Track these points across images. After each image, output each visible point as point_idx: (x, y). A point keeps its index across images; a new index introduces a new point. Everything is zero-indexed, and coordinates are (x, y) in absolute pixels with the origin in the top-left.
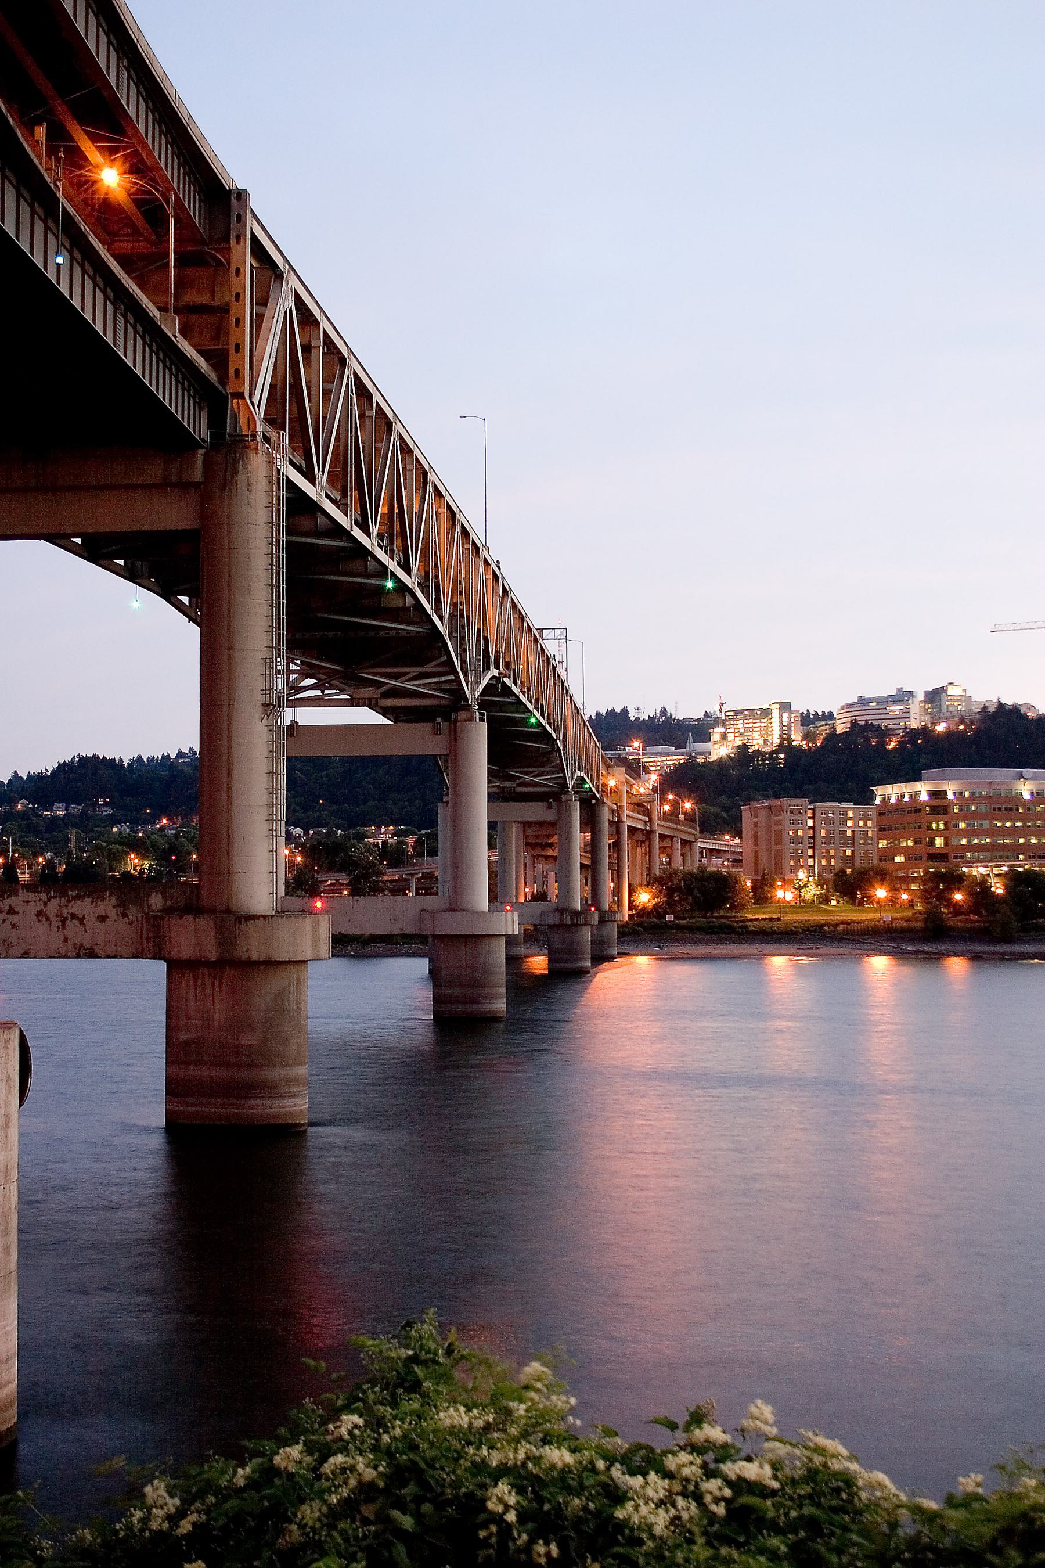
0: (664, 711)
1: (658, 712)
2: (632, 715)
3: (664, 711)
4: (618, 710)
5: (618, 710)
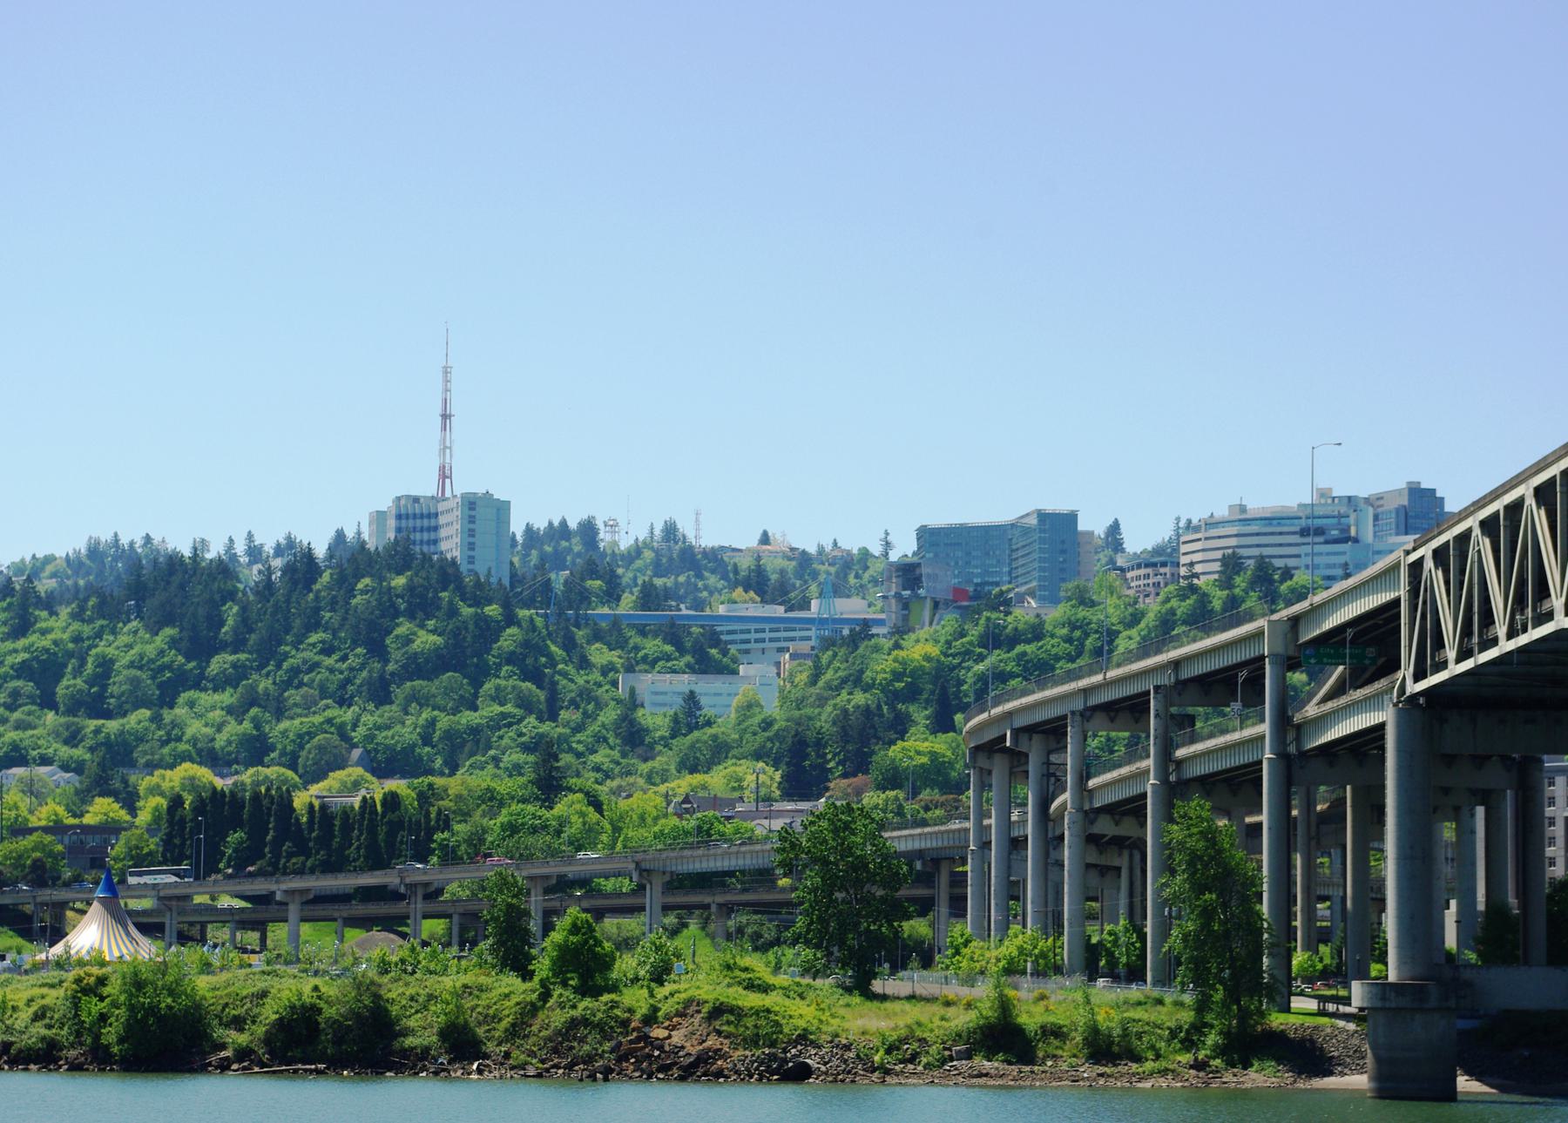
0: (670, 531)
1: (657, 532)
2: (604, 536)
3: (670, 531)
4: (573, 525)
5: (573, 525)
